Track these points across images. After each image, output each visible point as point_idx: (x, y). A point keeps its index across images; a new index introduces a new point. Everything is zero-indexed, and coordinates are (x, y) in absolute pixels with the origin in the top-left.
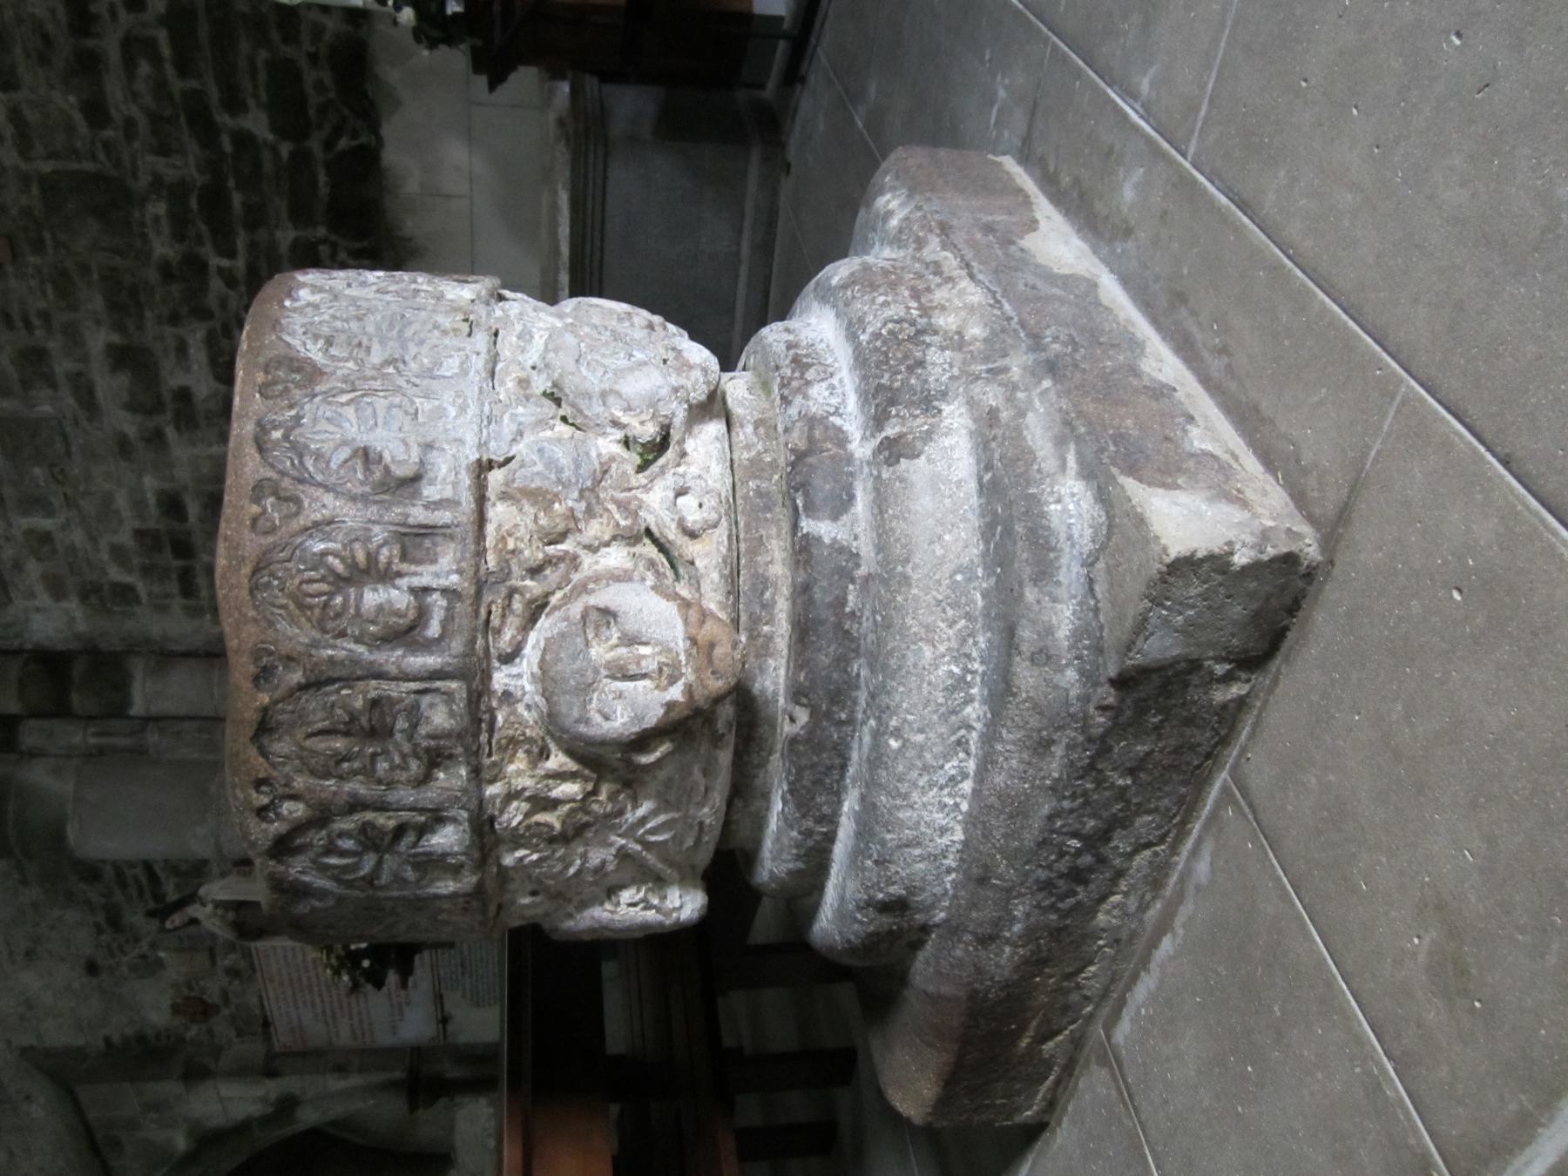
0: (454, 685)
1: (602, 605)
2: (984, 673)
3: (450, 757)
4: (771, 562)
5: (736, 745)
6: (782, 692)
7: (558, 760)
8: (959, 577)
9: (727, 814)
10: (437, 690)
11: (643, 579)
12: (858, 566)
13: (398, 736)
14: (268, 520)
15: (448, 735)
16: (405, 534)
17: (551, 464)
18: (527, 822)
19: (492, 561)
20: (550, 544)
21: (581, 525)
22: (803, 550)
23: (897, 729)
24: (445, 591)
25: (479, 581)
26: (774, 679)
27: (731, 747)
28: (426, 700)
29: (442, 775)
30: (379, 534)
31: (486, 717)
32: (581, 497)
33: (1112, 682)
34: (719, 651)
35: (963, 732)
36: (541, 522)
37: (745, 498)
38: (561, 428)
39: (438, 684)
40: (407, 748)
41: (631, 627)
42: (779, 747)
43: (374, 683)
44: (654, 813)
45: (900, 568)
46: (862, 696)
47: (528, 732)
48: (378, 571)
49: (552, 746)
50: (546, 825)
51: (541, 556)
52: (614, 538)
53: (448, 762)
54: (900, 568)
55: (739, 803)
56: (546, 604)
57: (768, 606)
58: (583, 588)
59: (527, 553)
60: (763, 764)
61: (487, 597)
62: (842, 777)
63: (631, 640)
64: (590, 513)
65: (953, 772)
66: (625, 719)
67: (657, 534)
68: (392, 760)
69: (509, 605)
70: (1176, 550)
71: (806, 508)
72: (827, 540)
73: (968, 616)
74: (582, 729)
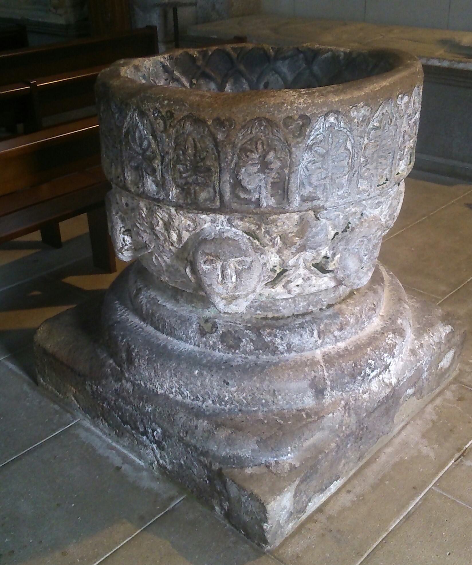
0: (218, 204)
2: (224, 410)
7: (186, 236)
8: (263, 401)
13: (194, 177)
14: (291, 123)
17: (317, 234)
23: (202, 374)
28: (211, 190)
33: (220, 469)
35: (201, 399)
36: (290, 234)
38: (333, 233)
39: (218, 197)
45: (267, 378)
54: (267, 378)
65: (185, 394)
67: (284, 274)
70: (269, 508)
73: (248, 404)
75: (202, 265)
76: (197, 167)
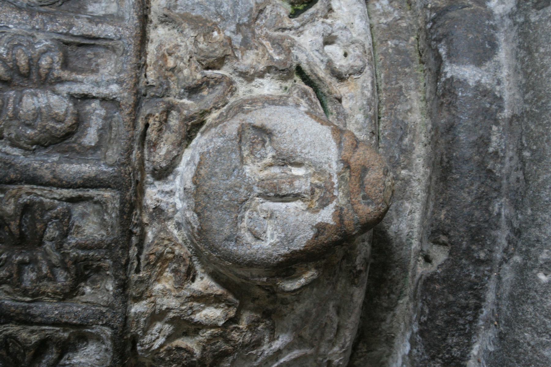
0: (107, 194)
1: (258, 123)
3: (98, 270)
4: (410, 111)
5: (368, 287)
6: (416, 235)
7: (202, 283)
9: (352, 356)
10: (90, 199)
11: (297, 105)
12: (501, 108)
13: (48, 245)
15: (98, 247)
16: (67, 44)
18: (169, 345)
19: (151, 75)
20: (208, 68)
21: (238, 54)
22: (444, 94)
24: (104, 100)
25: (137, 93)
26: (408, 223)
27: (365, 287)
28: (78, 209)
29: (88, 289)
30: (43, 42)
31: (137, 230)
32: (238, 30)
34: (371, 176)
37: (385, 54)
39: (92, 192)
40: (55, 258)
41: (286, 146)
42: (409, 290)
43: (27, 187)
44: (289, 347)
46: (502, 235)
47: (177, 250)
48: (39, 75)
49: (198, 268)
50: (187, 350)
51: (199, 76)
52: (269, 69)
53: (94, 276)
55: (363, 348)
56: (202, 123)
57: (407, 151)
58: (240, 108)
59: (186, 72)
60: (391, 308)
61: (145, 110)
62: (476, 317)
63: (285, 160)
64: (246, 45)
66: (275, 240)
67: (308, 72)
68: (40, 269)
69: (166, 121)
71: (449, 55)
72: (471, 83)
74: (232, 247)
75: (266, 245)
76: (22, 236)
